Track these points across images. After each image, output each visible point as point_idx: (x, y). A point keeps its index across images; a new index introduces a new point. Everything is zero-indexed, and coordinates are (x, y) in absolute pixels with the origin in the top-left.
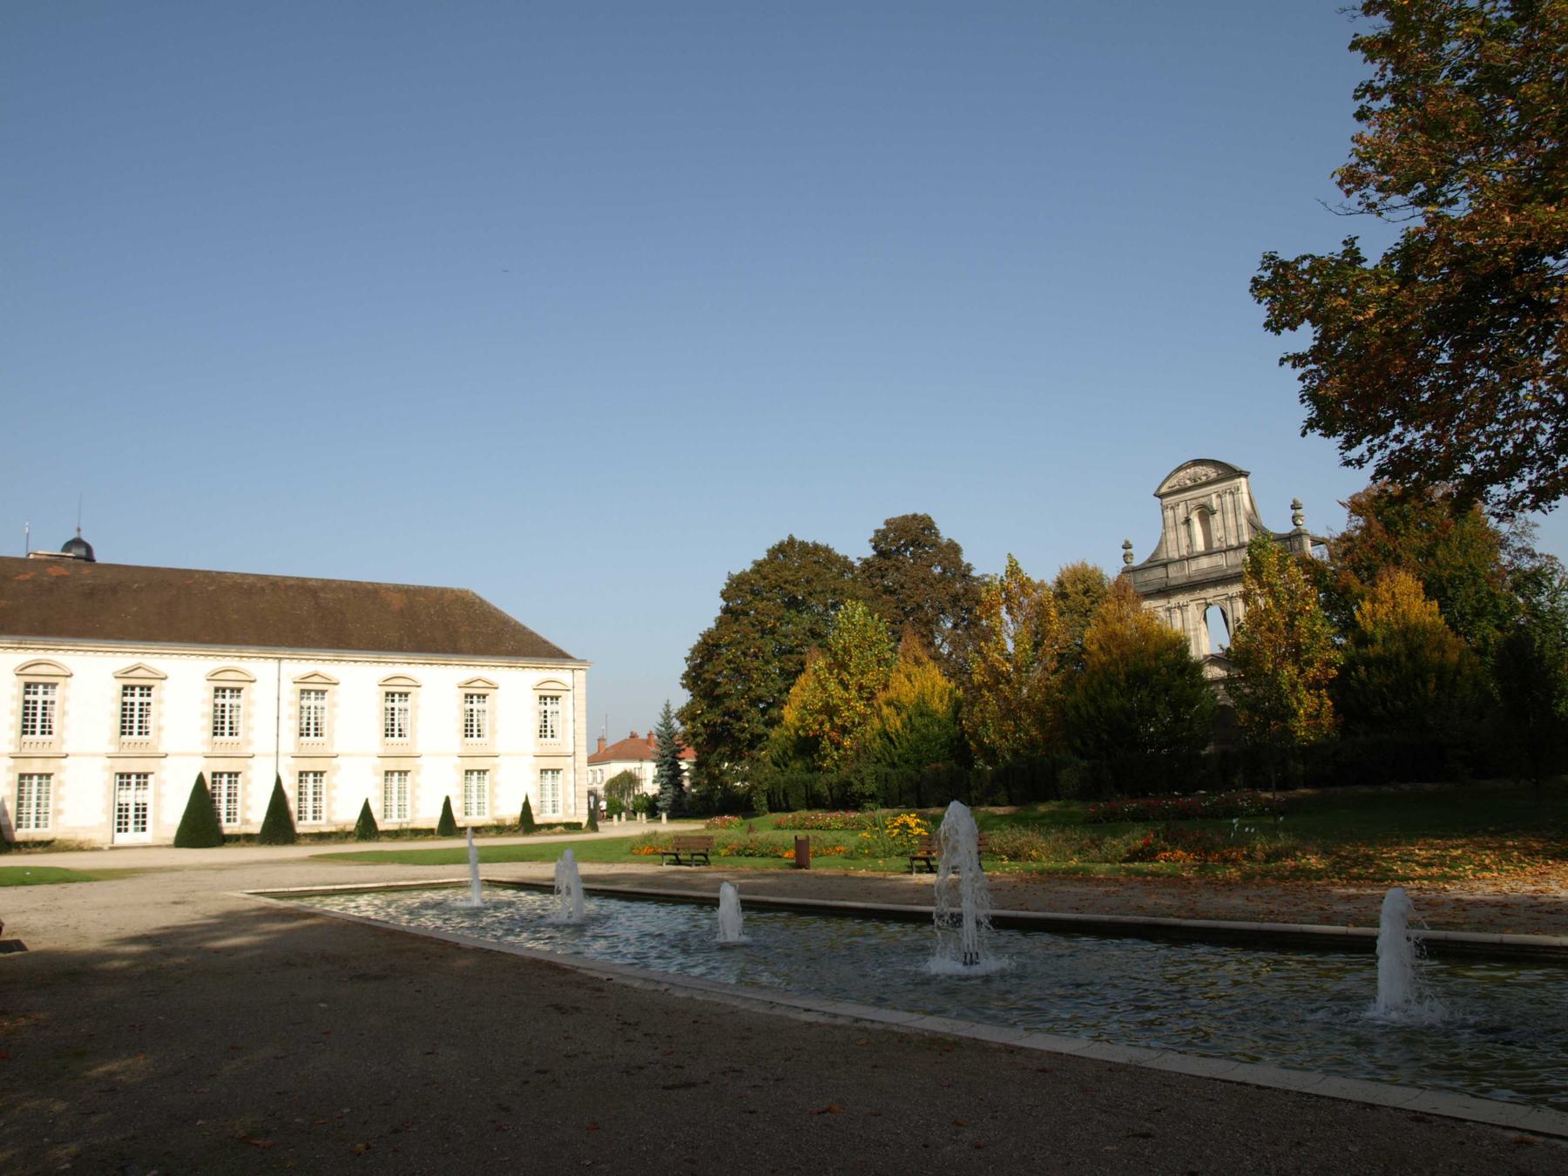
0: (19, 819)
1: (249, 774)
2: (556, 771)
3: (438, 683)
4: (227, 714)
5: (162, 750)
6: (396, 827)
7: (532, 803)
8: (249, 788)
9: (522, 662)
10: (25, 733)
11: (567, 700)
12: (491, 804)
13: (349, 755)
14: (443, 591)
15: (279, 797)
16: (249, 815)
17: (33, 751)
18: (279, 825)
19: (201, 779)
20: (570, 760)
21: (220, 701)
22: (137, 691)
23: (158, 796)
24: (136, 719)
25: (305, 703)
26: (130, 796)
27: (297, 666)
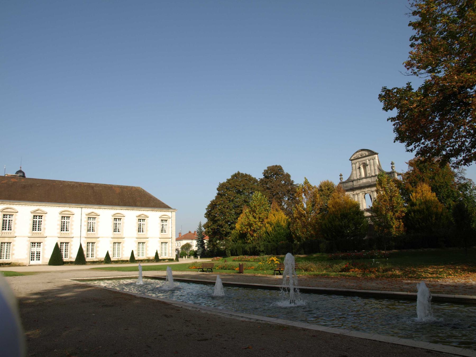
1: (72, 243)
2: (166, 243)
3: (130, 216)
4: (65, 224)
5: (45, 235)
6: (117, 260)
8: (72, 247)
9: (156, 209)
11: (169, 221)
13: (103, 237)
14: (132, 188)
15: (81, 250)
16: (72, 256)
17: (6, 235)
18: (81, 259)
19: (57, 244)
21: (63, 220)
22: (38, 217)
24: (37, 226)
25: (89, 221)
26: (35, 249)
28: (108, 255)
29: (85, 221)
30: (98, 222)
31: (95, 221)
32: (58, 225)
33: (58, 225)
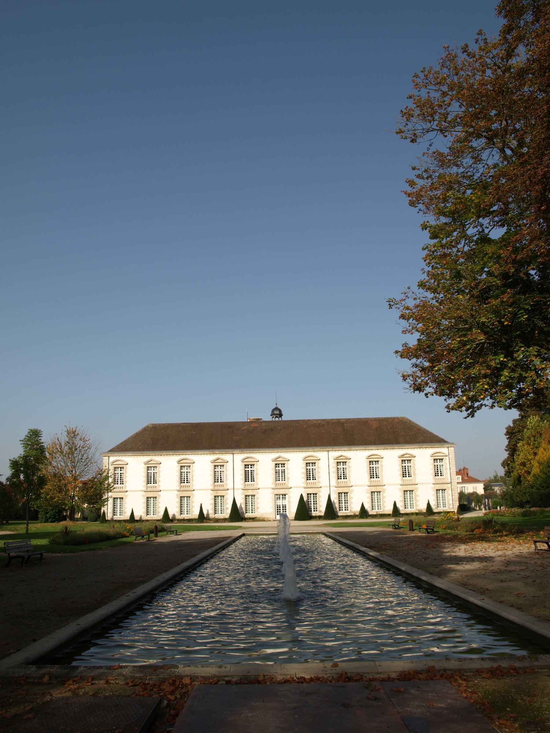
0: (340, 508)
1: (291, 495)
3: (390, 457)
4: (407, 469)
5: (290, 486)
7: (398, 505)
10: (215, 482)
11: (446, 461)
12: (416, 504)
14: (394, 419)
15: (330, 504)
16: (321, 509)
18: (331, 511)
19: (302, 496)
20: (449, 485)
21: (404, 465)
22: (280, 465)
23: (289, 502)
24: (250, 476)
25: (308, 468)
26: (280, 502)
27: (335, 453)
28: (363, 507)
29: (333, 467)
30: (349, 467)
31: (443, 463)
32: (303, 473)
33: (303, 473)
